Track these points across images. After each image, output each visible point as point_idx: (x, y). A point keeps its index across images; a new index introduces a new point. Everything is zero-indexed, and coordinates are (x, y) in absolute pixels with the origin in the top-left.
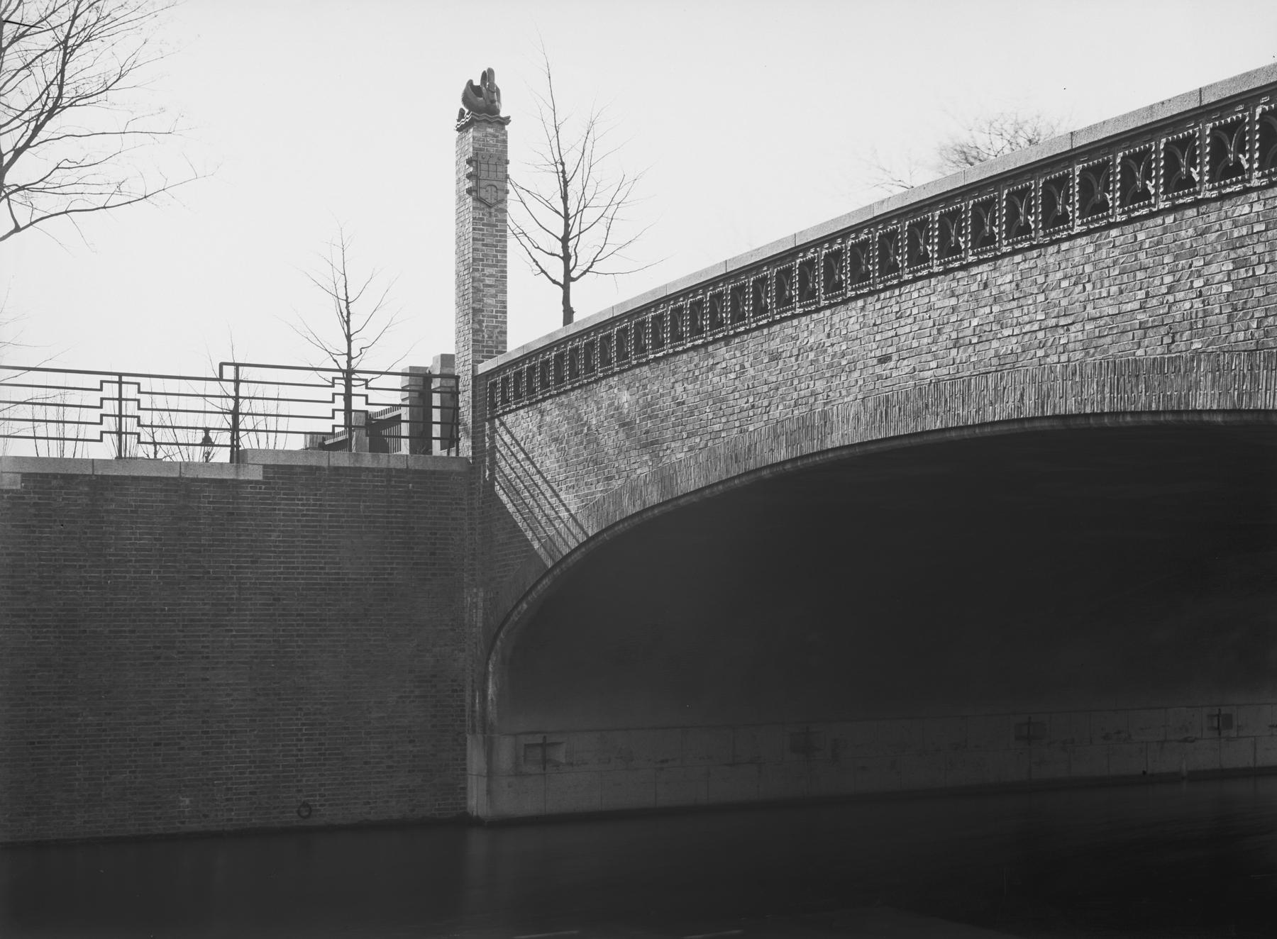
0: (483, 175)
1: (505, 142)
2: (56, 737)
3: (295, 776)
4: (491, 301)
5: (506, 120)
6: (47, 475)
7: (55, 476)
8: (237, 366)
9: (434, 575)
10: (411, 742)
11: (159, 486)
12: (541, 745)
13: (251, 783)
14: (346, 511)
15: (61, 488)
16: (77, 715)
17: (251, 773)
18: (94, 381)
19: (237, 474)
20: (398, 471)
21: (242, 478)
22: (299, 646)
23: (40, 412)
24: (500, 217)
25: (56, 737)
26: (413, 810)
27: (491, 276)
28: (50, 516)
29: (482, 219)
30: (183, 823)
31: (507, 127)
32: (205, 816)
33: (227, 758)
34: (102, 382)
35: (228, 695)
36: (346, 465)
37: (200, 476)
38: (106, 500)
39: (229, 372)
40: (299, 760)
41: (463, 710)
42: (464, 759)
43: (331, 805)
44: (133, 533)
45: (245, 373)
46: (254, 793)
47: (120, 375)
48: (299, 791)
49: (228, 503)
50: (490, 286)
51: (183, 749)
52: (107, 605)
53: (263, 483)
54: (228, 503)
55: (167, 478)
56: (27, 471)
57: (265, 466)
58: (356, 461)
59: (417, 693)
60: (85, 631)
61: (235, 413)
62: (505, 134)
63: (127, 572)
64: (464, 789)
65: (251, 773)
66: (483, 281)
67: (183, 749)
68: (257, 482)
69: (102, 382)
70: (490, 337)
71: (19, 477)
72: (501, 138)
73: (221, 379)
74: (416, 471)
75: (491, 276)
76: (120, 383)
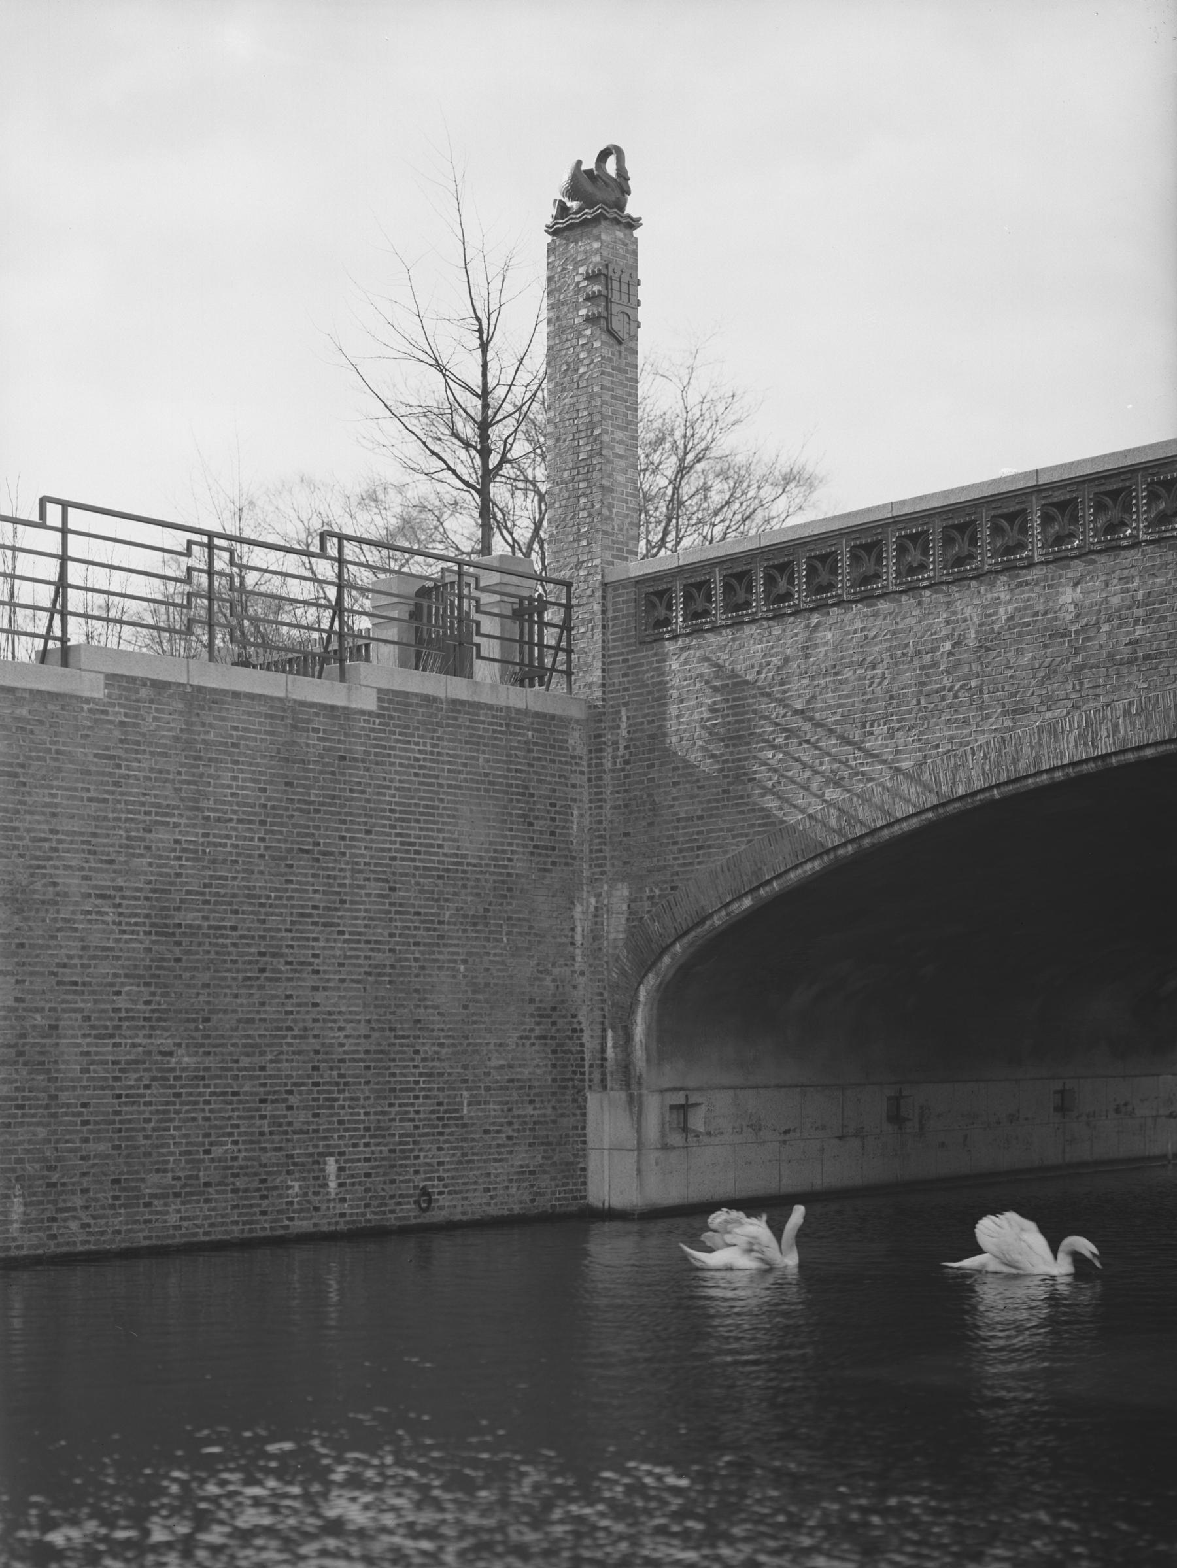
0: (615, 296)
1: (635, 253)
2: (147, 1087)
3: (412, 1150)
4: (620, 478)
5: (632, 224)
6: (134, 679)
7: (144, 682)
8: (65, 505)
9: (554, 863)
10: (532, 1102)
11: (263, 709)
12: (682, 1106)
13: (367, 1160)
14: (465, 765)
15: (152, 701)
16: (170, 1054)
17: (367, 1145)
18: (177, 540)
19: (349, 699)
20: (518, 711)
21: (353, 706)
22: (416, 960)
23: (117, 582)
24: (630, 360)
25: (147, 1087)
26: (533, 1201)
27: (621, 442)
28: (137, 743)
29: (611, 360)
30: (291, 1219)
31: (636, 233)
32: (316, 1209)
33: (340, 1122)
34: (190, 543)
35: (340, 1029)
36: (465, 698)
37: (309, 699)
38: (203, 725)
39: (54, 514)
40: (416, 1127)
41: (583, 1059)
42: (584, 1128)
43: (450, 1193)
44: (235, 779)
45: (77, 520)
46: (368, 1175)
47: (211, 535)
48: (417, 1172)
49: (340, 741)
50: (620, 456)
51: (290, 1108)
52: (205, 886)
53: (379, 716)
54: (340, 741)
55: (272, 698)
56: (384, 685)
57: (380, 691)
58: (475, 693)
59: (537, 1033)
60: (179, 925)
61: (62, 584)
62: (635, 241)
63: (228, 837)
64: (584, 1169)
65: (367, 1145)
66: (612, 448)
67: (290, 1108)
68: (370, 714)
69: (190, 543)
70: (621, 530)
71: (102, 677)
72: (631, 247)
73: (42, 524)
74: (537, 715)
75: (621, 442)
76: (211, 547)
